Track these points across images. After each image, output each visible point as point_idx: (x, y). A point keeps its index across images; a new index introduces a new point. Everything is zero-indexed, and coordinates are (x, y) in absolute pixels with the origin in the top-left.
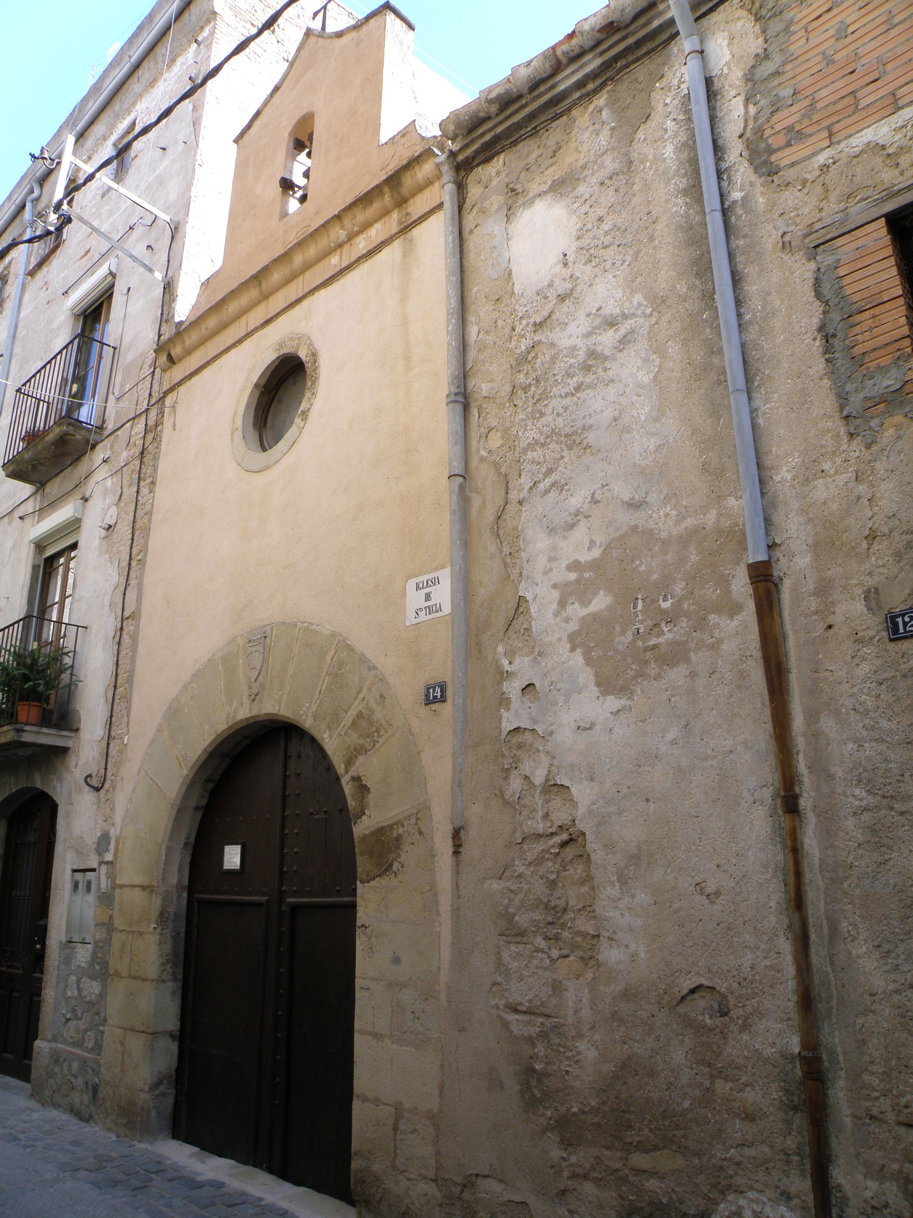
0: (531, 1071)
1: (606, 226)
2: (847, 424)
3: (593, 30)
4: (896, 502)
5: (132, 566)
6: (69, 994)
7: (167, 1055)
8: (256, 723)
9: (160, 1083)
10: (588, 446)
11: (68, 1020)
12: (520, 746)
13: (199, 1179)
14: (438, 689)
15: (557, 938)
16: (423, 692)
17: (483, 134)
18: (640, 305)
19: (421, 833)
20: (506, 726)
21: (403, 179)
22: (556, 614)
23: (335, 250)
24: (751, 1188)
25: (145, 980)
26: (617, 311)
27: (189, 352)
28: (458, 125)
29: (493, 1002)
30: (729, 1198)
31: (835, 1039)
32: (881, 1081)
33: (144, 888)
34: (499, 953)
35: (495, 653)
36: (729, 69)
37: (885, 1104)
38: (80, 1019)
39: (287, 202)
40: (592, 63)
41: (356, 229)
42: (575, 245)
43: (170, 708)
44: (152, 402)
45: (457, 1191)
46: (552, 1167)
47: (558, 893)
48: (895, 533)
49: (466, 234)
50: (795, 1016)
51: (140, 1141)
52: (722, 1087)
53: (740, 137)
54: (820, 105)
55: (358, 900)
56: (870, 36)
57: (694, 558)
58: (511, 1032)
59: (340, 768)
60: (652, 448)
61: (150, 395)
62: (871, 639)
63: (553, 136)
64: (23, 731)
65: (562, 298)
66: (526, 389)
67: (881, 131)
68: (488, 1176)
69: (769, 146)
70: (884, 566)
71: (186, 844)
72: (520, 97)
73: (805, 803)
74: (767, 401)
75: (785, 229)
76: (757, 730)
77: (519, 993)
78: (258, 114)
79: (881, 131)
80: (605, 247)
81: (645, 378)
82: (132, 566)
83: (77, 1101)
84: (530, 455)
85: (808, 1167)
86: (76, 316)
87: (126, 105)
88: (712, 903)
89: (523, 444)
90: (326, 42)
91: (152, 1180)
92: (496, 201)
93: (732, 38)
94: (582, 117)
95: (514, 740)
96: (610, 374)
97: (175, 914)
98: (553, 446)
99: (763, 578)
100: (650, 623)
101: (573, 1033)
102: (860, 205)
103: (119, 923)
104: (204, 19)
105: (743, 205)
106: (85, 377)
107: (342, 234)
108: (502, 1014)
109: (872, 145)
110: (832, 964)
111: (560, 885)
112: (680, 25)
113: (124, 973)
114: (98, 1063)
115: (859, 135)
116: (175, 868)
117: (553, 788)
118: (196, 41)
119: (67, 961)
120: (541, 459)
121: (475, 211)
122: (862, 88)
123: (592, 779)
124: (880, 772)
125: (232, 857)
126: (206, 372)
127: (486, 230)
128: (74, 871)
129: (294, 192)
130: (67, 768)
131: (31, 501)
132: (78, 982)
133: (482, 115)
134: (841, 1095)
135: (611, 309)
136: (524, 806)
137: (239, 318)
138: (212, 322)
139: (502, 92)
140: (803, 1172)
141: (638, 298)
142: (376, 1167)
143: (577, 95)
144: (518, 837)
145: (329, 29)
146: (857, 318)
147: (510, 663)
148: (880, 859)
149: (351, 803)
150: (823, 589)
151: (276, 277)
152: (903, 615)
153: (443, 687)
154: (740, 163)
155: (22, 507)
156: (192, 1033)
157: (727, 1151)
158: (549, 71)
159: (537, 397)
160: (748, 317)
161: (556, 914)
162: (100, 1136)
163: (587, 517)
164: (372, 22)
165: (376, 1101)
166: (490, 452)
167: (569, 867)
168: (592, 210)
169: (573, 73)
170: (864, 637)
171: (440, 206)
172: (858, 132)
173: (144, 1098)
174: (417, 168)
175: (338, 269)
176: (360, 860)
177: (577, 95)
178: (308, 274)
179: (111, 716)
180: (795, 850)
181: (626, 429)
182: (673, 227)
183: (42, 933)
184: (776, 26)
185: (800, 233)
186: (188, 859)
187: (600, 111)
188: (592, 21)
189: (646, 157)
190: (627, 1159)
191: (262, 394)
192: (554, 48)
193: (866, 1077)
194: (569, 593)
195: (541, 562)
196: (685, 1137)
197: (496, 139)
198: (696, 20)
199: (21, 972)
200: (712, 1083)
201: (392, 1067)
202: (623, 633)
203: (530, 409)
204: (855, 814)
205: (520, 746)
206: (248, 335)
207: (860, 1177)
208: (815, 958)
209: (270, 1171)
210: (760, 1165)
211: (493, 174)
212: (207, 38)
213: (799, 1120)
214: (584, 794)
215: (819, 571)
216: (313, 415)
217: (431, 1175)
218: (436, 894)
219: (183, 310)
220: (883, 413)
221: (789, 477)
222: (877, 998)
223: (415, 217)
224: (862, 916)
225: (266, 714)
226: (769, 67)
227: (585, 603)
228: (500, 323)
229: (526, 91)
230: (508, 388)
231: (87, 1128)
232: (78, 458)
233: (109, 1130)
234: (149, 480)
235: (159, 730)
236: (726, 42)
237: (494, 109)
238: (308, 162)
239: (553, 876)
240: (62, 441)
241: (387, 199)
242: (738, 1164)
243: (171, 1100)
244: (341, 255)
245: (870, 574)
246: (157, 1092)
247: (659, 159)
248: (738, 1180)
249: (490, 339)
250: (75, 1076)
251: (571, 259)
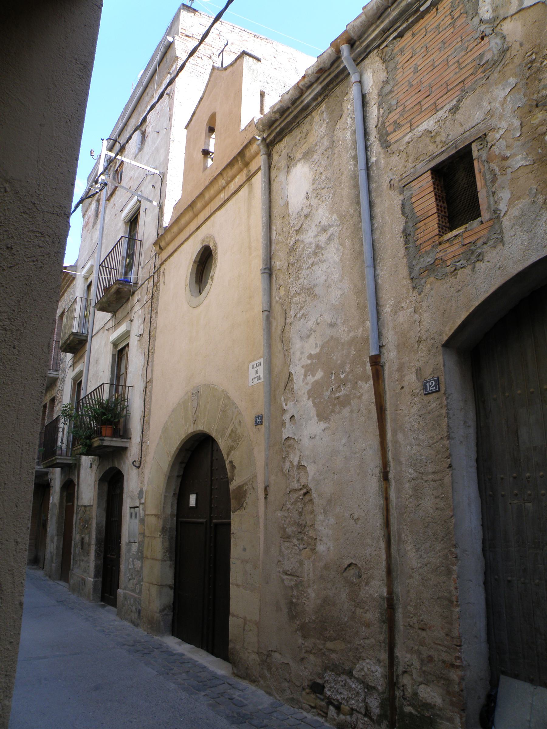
0: (291, 603)
1: (323, 177)
2: (412, 282)
3: (313, 73)
4: (429, 323)
5: (149, 356)
6: (130, 567)
7: (168, 596)
8: (200, 433)
9: (165, 609)
10: (315, 295)
11: (130, 579)
12: (289, 446)
13: (174, 652)
14: (260, 418)
15: (302, 539)
16: (254, 418)
17: (276, 128)
18: (335, 220)
19: (253, 488)
20: (284, 437)
21: (246, 153)
22: (303, 381)
24: (368, 658)
25: (157, 560)
26: (327, 223)
27: (168, 244)
28: (263, 125)
29: (278, 570)
30: (360, 662)
31: (399, 590)
32: (414, 609)
33: (156, 515)
34: (280, 546)
35: (281, 400)
36: (372, 89)
37: (415, 620)
38: (134, 579)
40: (317, 88)
41: (229, 179)
42: (312, 187)
43: (164, 427)
44: (156, 270)
45: (265, 658)
46: (299, 647)
47: (302, 518)
48: (428, 339)
49: (272, 181)
50: (385, 578)
51: (156, 636)
52: (359, 611)
53: (376, 127)
54: (407, 109)
55: (232, 521)
56: (426, 72)
57: (353, 352)
58: (285, 584)
59: (225, 456)
60: (339, 296)
61: (155, 266)
62: (418, 394)
63: (305, 127)
64: (104, 440)
65: (306, 216)
66: (293, 265)
67: (429, 124)
68: (275, 651)
69: (387, 131)
70: (423, 357)
71: (174, 494)
72: (288, 108)
73: (391, 476)
74: (382, 270)
75: (392, 177)
76: (374, 440)
77: (288, 565)
78: (194, 113)
79: (429, 124)
80: (323, 189)
81: (337, 259)
82: (149, 356)
83: (133, 617)
84: (295, 299)
85: (387, 648)
86: (126, 223)
87: (143, 108)
88: (356, 524)
89: (292, 294)
91: (154, 651)
92: (283, 163)
93: (374, 72)
94: (316, 116)
95: (287, 443)
96: (324, 256)
97: (170, 528)
98: (303, 295)
99: (376, 362)
100: (337, 385)
101: (307, 585)
102: (421, 164)
103: (147, 533)
105: (376, 165)
106: (133, 254)
108: (282, 576)
109: (427, 130)
110: (399, 554)
111: (303, 514)
112: (350, 70)
113: (149, 557)
114: (140, 600)
115: (421, 125)
116: (169, 506)
117: (301, 467)
118: (169, 73)
119: (129, 551)
120: (298, 302)
121: (275, 168)
122: (423, 100)
123: (315, 463)
124: (419, 461)
125: (193, 500)
126: (176, 254)
127: (279, 178)
128: (131, 508)
130: (127, 457)
131: (111, 321)
132: (133, 561)
133: (273, 119)
134: (400, 615)
135: (325, 223)
136: (291, 476)
138: (175, 229)
139: (279, 107)
140: (385, 650)
141: (335, 216)
142: (237, 647)
143: (314, 104)
144: (288, 490)
146: (419, 225)
147: (286, 405)
148: (417, 504)
149: (229, 474)
150: (400, 369)
151: (199, 205)
152: (429, 382)
153: (261, 417)
154: (375, 142)
155: (108, 324)
156: (178, 586)
157: (360, 641)
158: (298, 95)
159: (297, 269)
160: (376, 226)
161: (302, 527)
162: (141, 633)
163: (315, 331)
164: (238, 61)
165: (237, 616)
166: (280, 298)
167: (307, 505)
168: (318, 168)
169: (310, 94)
170: (415, 393)
171: (259, 168)
172: (421, 124)
173: (157, 616)
176: (232, 501)
177: (314, 104)
179: (143, 431)
180: (387, 499)
181: (329, 286)
182: (349, 177)
183: (119, 537)
184: (392, 65)
185: (397, 179)
186: (176, 501)
187: (323, 113)
188: (312, 69)
189: (340, 138)
190: (325, 644)
191: (198, 266)
192: (298, 83)
193: (409, 607)
194: (309, 370)
195: (298, 354)
196: (345, 634)
197: (282, 130)
198: (357, 65)
199: (115, 557)
200: (355, 610)
201: (244, 601)
202: (327, 390)
203: (294, 276)
204: (409, 481)
205: (289, 446)
206: (191, 235)
207: (404, 652)
208: (393, 551)
209: (208, 651)
210: (371, 647)
211: (283, 148)
213: (385, 627)
214: (311, 469)
215: (399, 359)
216: (215, 278)
217: (256, 650)
218: (258, 518)
219: (167, 221)
220: (427, 276)
221: (389, 310)
222: (414, 571)
223: (252, 173)
224: (410, 532)
225: (199, 430)
226: (388, 88)
227: (313, 376)
228: (284, 229)
229: (290, 105)
230: (286, 264)
231: (136, 629)
232: (128, 299)
233: (145, 630)
234: (155, 311)
235: (160, 438)
236: (371, 74)
237: (277, 116)
239: (300, 510)
240: (118, 292)
241: (240, 163)
242: (363, 647)
243: (170, 618)
245: (418, 361)
246: (164, 613)
247: (345, 140)
248: (364, 655)
249: (281, 238)
250: (132, 606)
251: (310, 195)
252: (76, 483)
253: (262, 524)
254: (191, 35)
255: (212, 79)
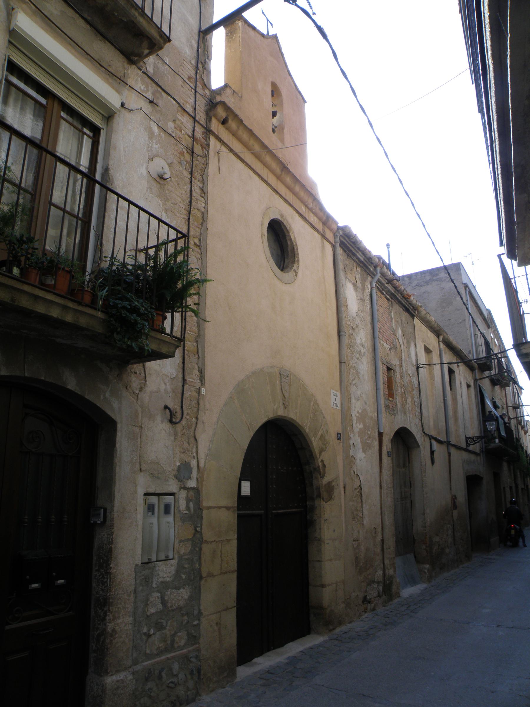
27: (234, 134)
59: (318, 455)
225: (291, 418)
252: (386, 460)
253: (343, 511)
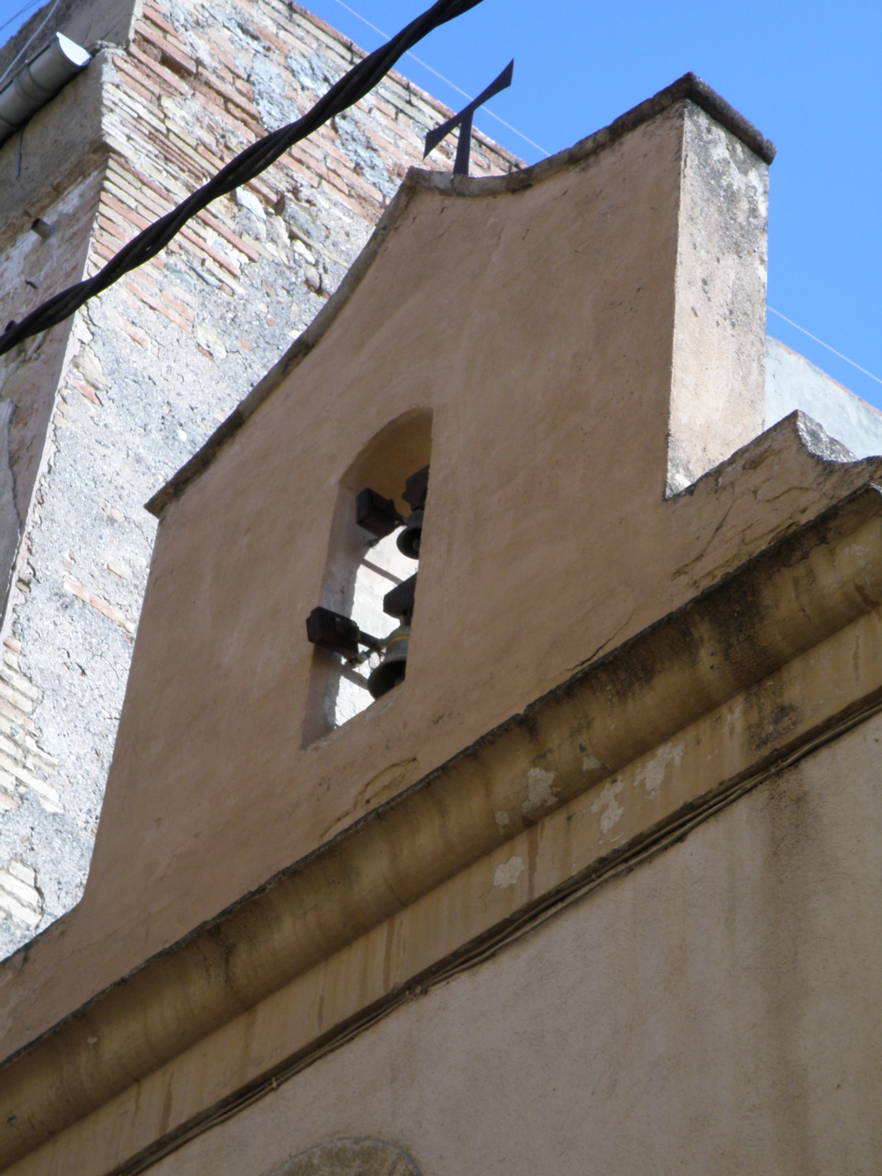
21: (767, 594)
23: (509, 837)
39: (332, 691)
41: (590, 764)
90: (477, 207)
104: (66, 166)
107: (539, 782)
129: (355, 660)
137: (137, 1080)
145: (480, 167)
151: (288, 931)
164: (633, 140)
174: (818, 558)
175: (520, 901)
178: (405, 922)
212: (72, 217)
223: (802, 729)
238: (405, 567)
241: (708, 661)
244: (533, 853)
254: (191, 66)
255: (392, 243)
